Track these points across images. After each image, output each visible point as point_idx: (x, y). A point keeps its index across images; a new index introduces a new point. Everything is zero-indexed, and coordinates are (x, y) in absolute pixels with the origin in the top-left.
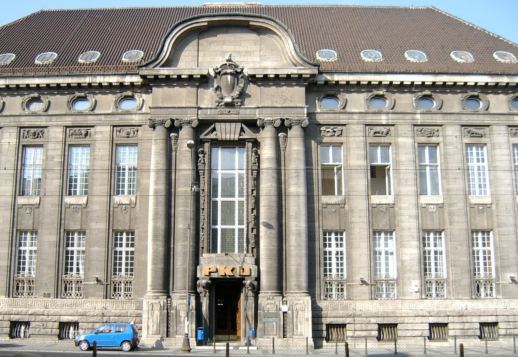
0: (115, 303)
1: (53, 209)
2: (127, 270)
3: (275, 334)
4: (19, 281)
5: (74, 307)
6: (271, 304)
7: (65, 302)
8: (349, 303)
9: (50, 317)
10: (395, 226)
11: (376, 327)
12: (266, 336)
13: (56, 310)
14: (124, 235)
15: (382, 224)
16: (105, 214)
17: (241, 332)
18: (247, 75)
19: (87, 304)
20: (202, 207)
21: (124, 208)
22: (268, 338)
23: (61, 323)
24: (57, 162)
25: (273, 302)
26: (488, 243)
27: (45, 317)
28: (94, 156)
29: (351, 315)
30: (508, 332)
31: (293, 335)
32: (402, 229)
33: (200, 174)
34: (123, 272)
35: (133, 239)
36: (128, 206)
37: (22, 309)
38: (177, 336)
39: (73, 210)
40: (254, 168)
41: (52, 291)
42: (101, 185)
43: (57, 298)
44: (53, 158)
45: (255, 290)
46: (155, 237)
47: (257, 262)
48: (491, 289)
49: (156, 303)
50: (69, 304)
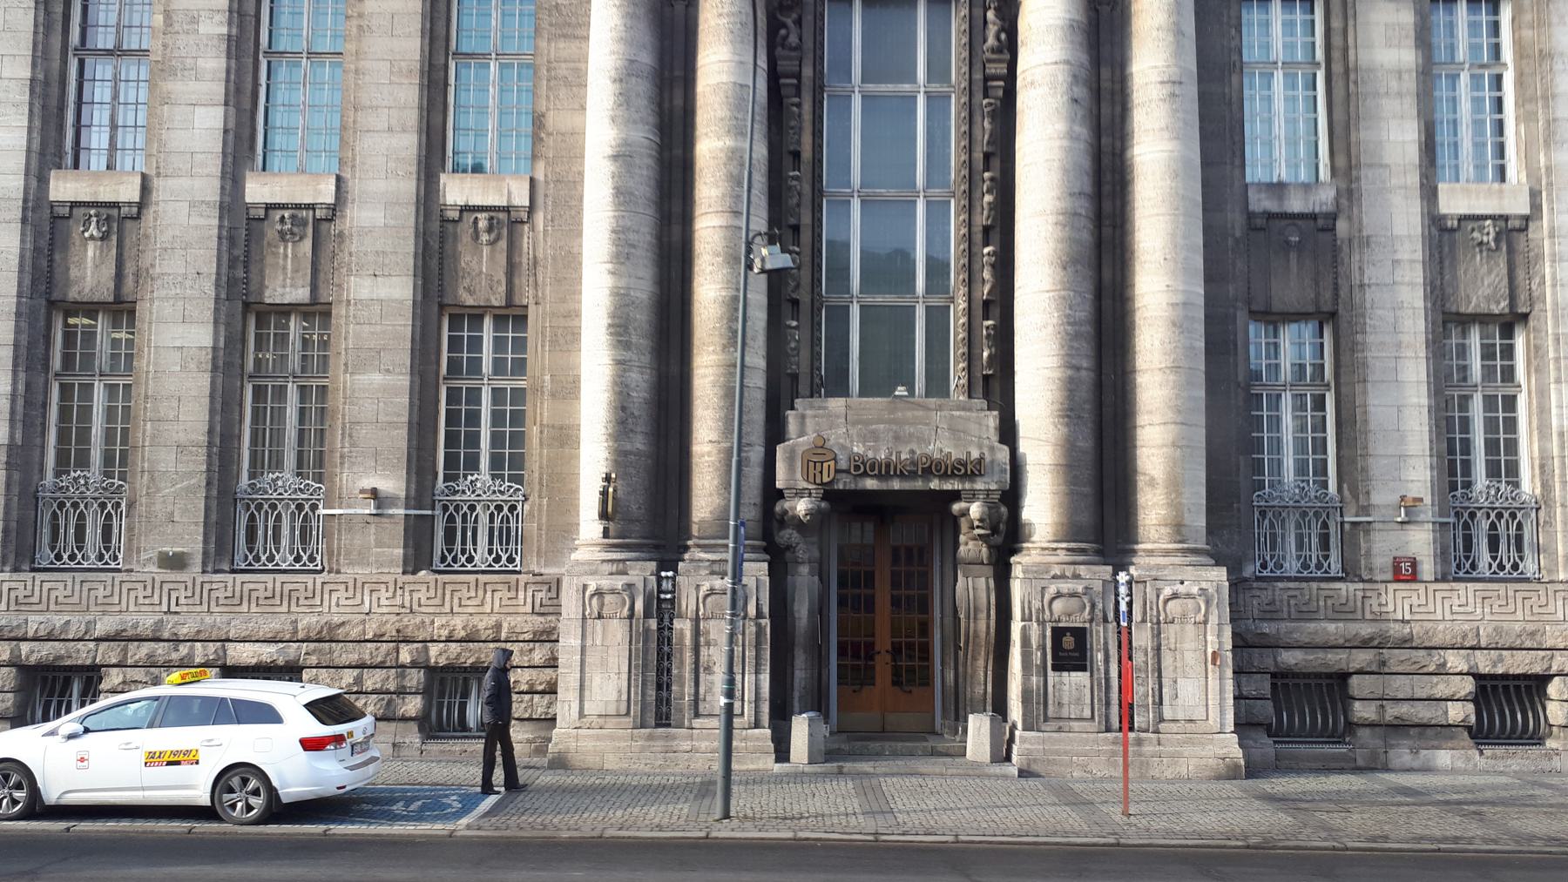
0: (449, 588)
1: (196, 220)
2: (496, 463)
3: (1087, 713)
4: (1500, 516)
5: (284, 608)
6: (1073, 595)
7: (287, 587)
8: (1360, 594)
9: (184, 649)
10: (1531, 301)
11: (1468, 686)
12: (1053, 725)
13: (208, 620)
14: (488, 323)
15: (1482, 287)
16: (405, 249)
17: (878, 680)
18: (1013, 559)
19: (497, 595)
20: (763, 622)
21: (482, 224)
22: (1060, 730)
23: (432, 671)
24: (210, 37)
25: (1080, 589)
26: (1304, 451)
27: (160, 649)
28: (360, 15)
29: (1372, 639)
30: (230, 652)
31: (1162, 720)
32: (157, 204)
33: (784, 92)
34: (484, 475)
35: (521, 345)
36: (502, 216)
37: (67, 618)
38: (697, 723)
39: (278, 227)
40: (992, 69)
41: (192, 542)
42: (390, 129)
43: (1458, 180)
44: (194, 20)
45: (998, 539)
46: (620, 329)
47: (1008, 432)
48: (1325, 543)
49: (613, 591)
50: (262, 594)
